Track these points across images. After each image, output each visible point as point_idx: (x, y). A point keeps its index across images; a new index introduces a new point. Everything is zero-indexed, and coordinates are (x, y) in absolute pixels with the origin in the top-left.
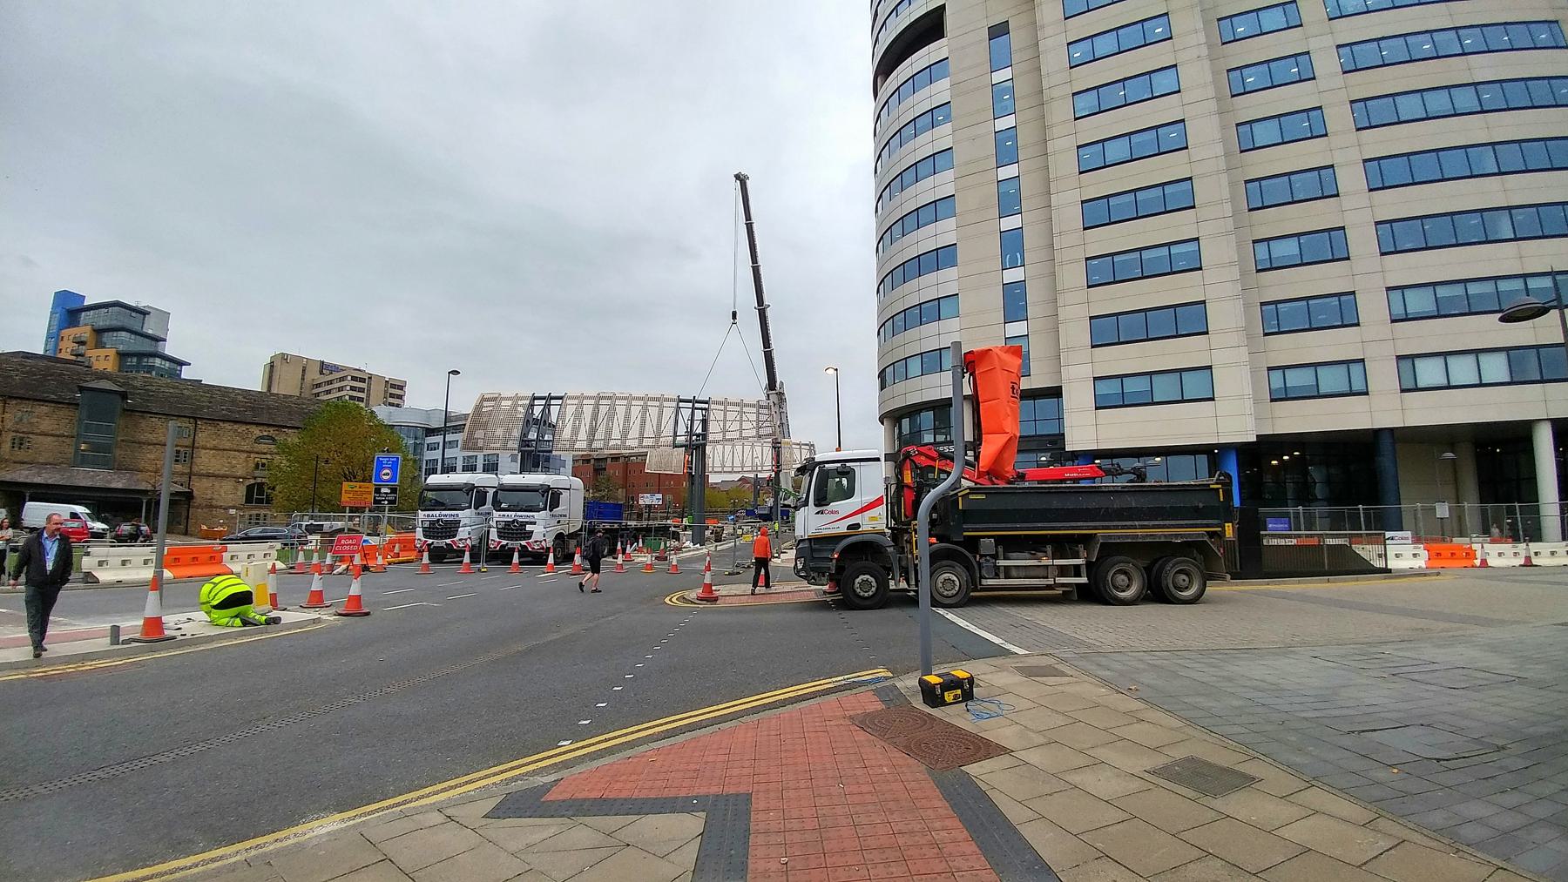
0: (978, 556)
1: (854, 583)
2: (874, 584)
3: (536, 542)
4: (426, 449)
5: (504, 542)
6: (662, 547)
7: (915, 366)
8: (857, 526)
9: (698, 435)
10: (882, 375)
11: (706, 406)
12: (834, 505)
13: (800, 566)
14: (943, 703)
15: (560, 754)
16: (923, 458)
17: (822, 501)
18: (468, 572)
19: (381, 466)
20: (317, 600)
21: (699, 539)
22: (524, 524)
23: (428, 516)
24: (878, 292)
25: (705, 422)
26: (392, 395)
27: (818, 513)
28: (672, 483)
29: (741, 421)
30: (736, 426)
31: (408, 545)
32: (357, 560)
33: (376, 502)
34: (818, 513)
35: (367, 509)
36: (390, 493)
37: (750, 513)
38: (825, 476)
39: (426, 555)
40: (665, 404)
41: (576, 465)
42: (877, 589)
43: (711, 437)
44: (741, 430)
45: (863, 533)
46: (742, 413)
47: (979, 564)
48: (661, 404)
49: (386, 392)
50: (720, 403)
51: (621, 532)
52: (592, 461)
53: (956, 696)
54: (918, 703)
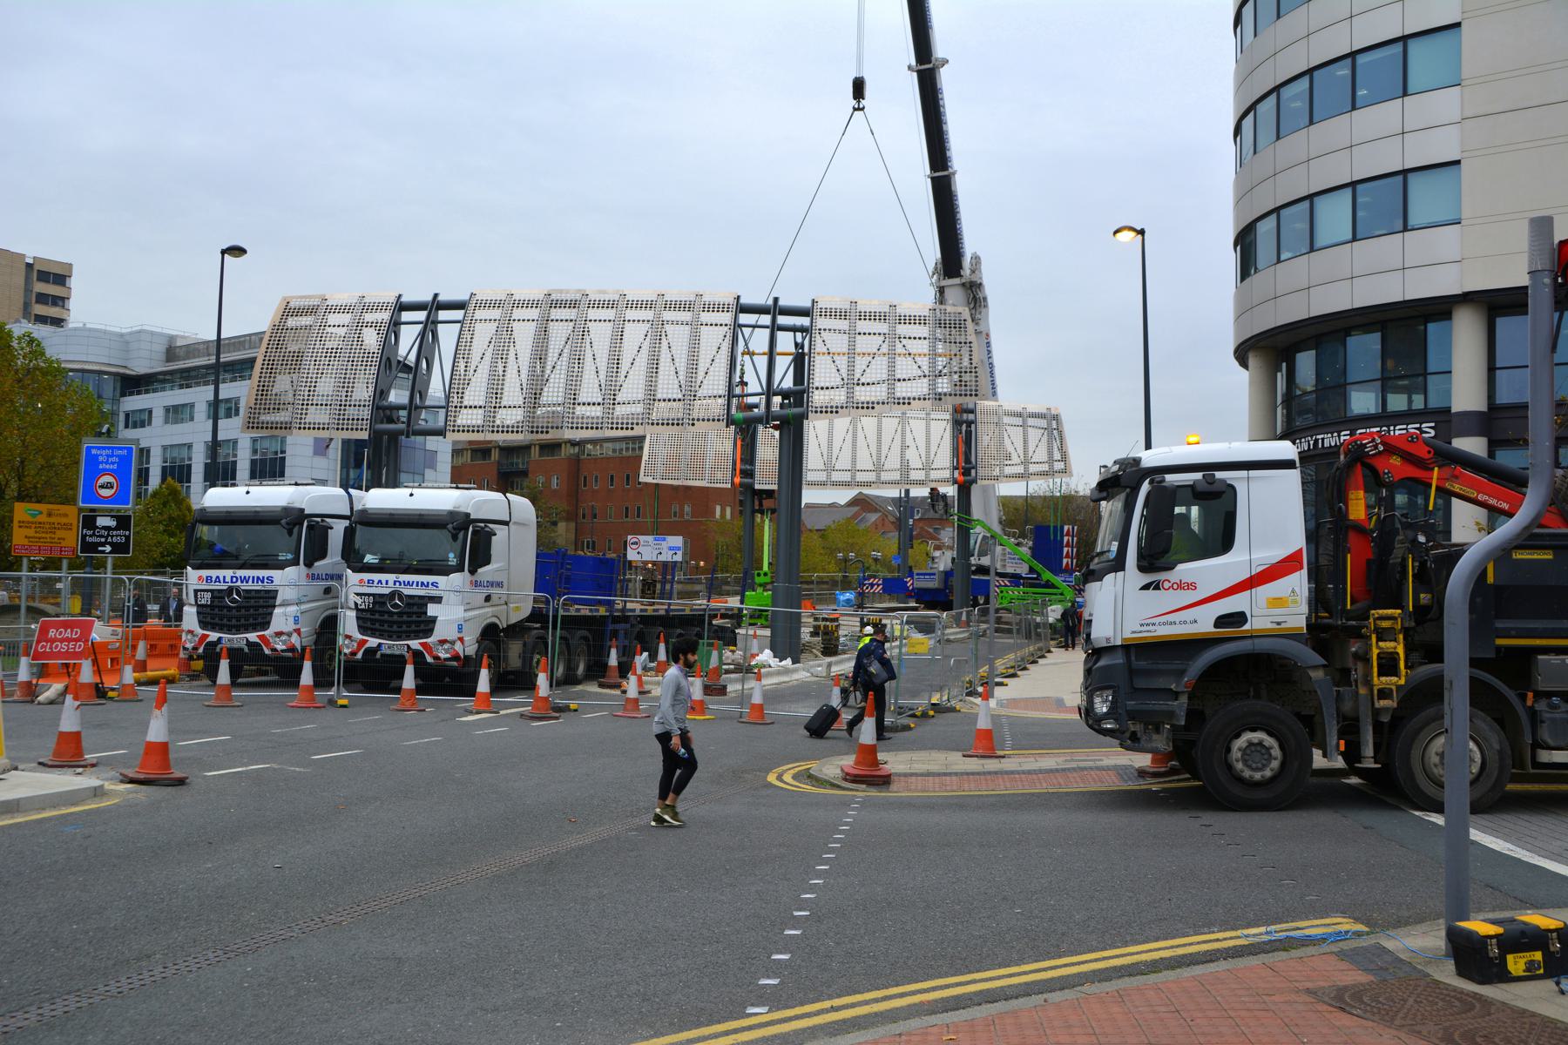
0: (1530, 695)
1: (1229, 750)
2: (1276, 752)
3: (443, 642)
4: (121, 424)
5: (373, 642)
6: (714, 662)
7: (1335, 216)
8: (1238, 618)
9: (785, 395)
10: (1245, 240)
11: (805, 321)
12: (1186, 570)
13: (1101, 707)
14: (1505, 977)
15: (750, 1028)
16: (1395, 461)
17: (1155, 560)
18: (311, 705)
19: (94, 471)
20: (69, 753)
21: (788, 647)
22: (423, 601)
23: (209, 579)
24: (1238, 20)
25: (800, 362)
26: (42, 299)
27: (1146, 587)
28: (687, 509)
29: (892, 356)
30: (879, 370)
31: (161, 644)
32: (87, 674)
33: (88, 547)
34: (1146, 587)
35: (65, 563)
36: (116, 529)
37: (894, 587)
38: (1163, 499)
39: (224, 666)
40: (706, 317)
41: (460, 461)
42: (1283, 764)
43: (818, 398)
44: (893, 380)
45: (1252, 636)
46: (892, 338)
47: (1534, 715)
48: (853, 327)
49: (28, 289)
50: (841, 315)
51: (611, 627)
52: (495, 455)
53: (1531, 965)
54: (1446, 974)
